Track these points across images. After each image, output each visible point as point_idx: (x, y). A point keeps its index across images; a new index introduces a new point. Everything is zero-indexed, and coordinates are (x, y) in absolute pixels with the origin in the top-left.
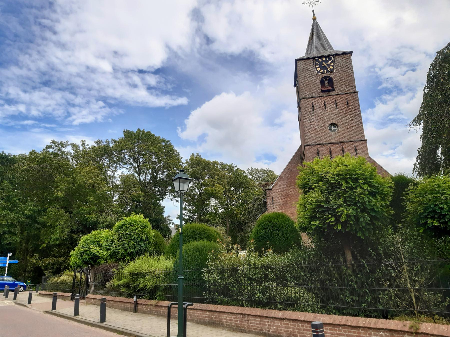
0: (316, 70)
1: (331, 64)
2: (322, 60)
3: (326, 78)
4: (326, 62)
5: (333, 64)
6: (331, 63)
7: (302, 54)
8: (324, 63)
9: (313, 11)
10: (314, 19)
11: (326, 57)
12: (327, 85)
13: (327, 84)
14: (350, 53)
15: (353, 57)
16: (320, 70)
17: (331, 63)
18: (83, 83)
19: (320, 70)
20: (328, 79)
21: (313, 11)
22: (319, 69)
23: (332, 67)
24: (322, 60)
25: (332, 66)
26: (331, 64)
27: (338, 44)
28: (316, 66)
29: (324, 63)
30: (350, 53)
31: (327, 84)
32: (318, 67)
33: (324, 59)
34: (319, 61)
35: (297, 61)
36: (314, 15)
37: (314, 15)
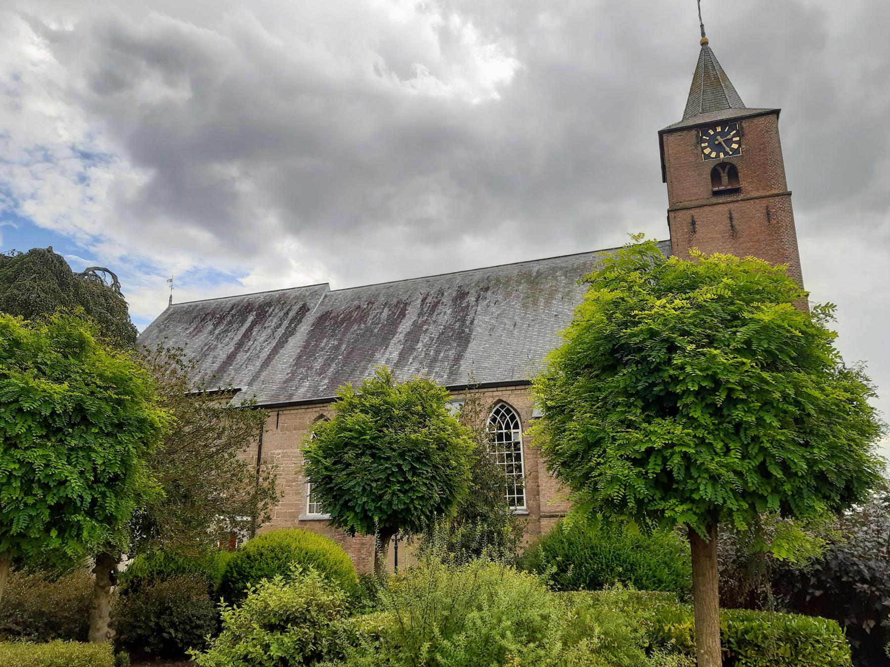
0: (703, 152)
1: (734, 139)
2: (715, 130)
3: (723, 165)
4: (722, 134)
5: (738, 139)
6: (734, 136)
7: (676, 115)
8: (719, 137)
9: (702, 26)
10: (704, 43)
11: (723, 123)
12: (725, 179)
13: (725, 179)
14: (777, 112)
15: (792, 197)
16: (711, 153)
17: (734, 136)
18: (378, 72)
19: (711, 153)
20: (728, 166)
21: (702, 26)
22: (707, 151)
23: (735, 146)
24: (715, 130)
25: (735, 142)
26: (734, 139)
27: (749, 94)
28: (703, 145)
29: (719, 137)
30: (777, 112)
31: (725, 179)
32: (705, 148)
33: (719, 129)
34: (709, 135)
35: (661, 134)
36: (703, 34)
37: (703, 34)
